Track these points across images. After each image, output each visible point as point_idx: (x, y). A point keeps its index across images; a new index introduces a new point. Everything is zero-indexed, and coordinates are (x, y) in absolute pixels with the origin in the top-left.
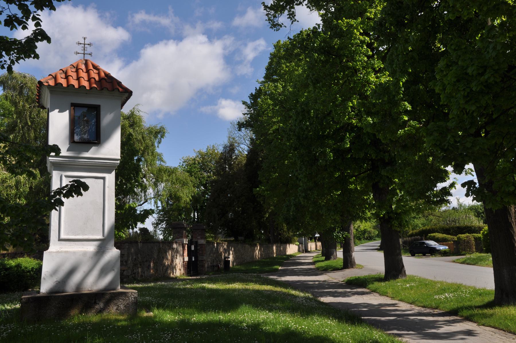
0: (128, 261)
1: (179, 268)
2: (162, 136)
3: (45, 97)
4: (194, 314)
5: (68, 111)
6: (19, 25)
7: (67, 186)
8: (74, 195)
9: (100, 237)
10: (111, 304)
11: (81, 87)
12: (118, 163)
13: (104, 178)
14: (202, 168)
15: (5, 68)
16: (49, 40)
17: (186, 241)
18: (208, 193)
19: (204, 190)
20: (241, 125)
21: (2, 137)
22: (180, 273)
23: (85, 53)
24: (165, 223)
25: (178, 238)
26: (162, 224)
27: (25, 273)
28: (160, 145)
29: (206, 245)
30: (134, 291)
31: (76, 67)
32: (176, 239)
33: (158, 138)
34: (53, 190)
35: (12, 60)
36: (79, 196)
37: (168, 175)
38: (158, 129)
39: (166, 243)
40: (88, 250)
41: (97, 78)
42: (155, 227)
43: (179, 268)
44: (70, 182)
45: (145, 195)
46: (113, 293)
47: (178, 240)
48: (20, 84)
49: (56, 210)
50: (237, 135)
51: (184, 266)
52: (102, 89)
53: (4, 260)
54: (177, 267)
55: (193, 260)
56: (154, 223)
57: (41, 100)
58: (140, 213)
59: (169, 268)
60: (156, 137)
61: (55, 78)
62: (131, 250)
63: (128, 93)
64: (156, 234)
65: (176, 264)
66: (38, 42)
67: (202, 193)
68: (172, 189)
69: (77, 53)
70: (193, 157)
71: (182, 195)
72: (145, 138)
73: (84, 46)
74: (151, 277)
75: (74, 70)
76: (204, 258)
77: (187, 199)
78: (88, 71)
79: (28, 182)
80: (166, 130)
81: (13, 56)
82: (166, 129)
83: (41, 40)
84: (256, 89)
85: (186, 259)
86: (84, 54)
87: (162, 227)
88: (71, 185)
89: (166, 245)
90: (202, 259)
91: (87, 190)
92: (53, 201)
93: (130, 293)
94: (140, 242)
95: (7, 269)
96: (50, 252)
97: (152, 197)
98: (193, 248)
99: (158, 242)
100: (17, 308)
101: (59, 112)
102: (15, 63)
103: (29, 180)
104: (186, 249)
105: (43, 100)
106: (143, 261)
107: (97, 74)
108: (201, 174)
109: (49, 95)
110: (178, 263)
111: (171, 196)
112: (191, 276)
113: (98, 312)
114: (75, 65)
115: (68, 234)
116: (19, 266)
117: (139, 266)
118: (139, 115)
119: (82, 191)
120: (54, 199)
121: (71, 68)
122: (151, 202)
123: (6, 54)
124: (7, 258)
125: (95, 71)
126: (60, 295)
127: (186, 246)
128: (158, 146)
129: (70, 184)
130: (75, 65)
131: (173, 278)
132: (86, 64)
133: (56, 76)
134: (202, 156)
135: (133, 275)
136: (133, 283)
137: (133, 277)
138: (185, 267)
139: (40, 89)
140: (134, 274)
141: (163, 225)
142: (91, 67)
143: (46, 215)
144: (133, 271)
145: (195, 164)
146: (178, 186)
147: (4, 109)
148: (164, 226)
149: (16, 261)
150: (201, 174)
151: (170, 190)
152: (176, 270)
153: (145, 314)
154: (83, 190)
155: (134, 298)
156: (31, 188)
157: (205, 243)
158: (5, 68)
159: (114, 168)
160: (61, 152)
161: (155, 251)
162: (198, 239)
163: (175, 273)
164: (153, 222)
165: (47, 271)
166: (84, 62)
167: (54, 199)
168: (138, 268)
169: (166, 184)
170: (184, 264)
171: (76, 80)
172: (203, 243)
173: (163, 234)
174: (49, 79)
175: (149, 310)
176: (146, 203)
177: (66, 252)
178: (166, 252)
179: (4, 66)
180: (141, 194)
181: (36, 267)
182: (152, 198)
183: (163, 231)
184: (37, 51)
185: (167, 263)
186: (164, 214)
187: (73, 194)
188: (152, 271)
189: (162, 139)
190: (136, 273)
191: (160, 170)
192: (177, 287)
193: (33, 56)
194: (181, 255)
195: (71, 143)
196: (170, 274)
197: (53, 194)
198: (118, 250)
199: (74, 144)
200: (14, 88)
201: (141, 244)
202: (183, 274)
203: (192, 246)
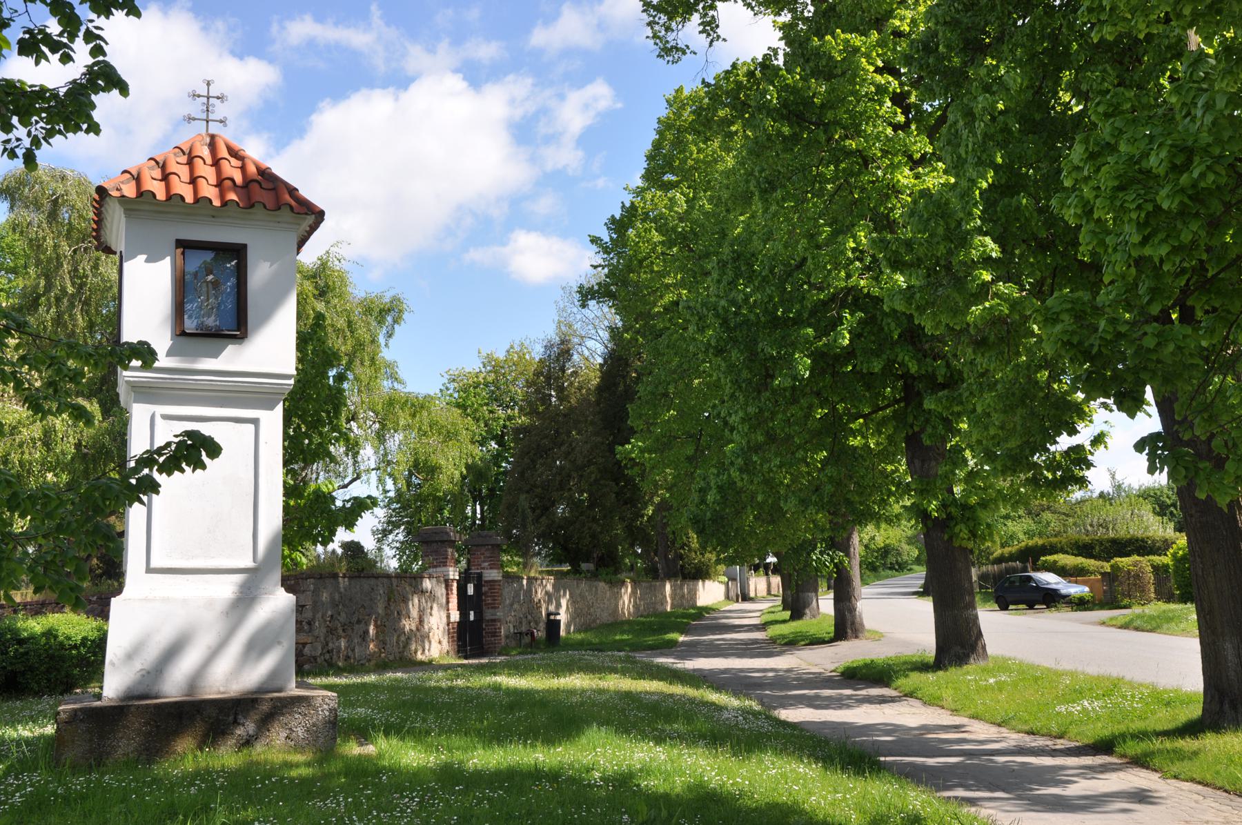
3: (112, 222)
5: (168, 259)
6: (54, 51)
7: (168, 444)
12: (290, 385)
13: (255, 422)
16: (123, 89)
17: (453, 574)
20: (586, 295)
25: (435, 567)
28: (391, 341)
31: (187, 152)
35: (36, 136)
36: (199, 471)
38: (386, 303)
41: (238, 178)
42: (379, 541)
45: (355, 462)
49: (142, 502)
50: (579, 317)
52: (252, 206)
57: (102, 232)
60: (381, 322)
61: (138, 179)
63: (313, 216)
69: (190, 119)
71: (442, 462)
74: (369, 660)
75: (184, 159)
78: (216, 163)
80: (405, 306)
81: (38, 126)
83: (106, 89)
84: (623, 206)
85: (455, 616)
88: (178, 444)
90: (493, 617)
92: (133, 481)
94: (344, 574)
95: (21, 642)
97: (373, 466)
98: (471, 590)
101: (147, 261)
104: (455, 591)
109: (123, 219)
110: (435, 627)
116: (52, 634)
121: (175, 154)
122: (368, 479)
123: (20, 122)
125: (234, 162)
127: (455, 584)
128: (386, 345)
129: (177, 440)
131: (422, 663)
132: (213, 145)
135: (327, 656)
136: (327, 675)
139: (101, 206)
140: (328, 652)
142: (223, 153)
146: (433, 440)
147: (13, 255)
148: (401, 537)
152: (430, 642)
156: (78, 446)
157: (500, 578)
162: (484, 568)
166: (208, 140)
168: (339, 638)
171: (189, 183)
172: (496, 578)
174: (122, 183)
177: (165, 600)
178: (405, 600)
181: (93, 635)
183: (397, 548)
184: (96, 115)
185: (407, 628)
187: (184, 465)
189: (396, 326)
190: (332, 650)
191: (391, 402)
192: (433, 684)
193: (85, 126)
194: (441, 606)
196: (416, 652)
197: (132, 464)
199: (182, 339)
201: (346, 579)
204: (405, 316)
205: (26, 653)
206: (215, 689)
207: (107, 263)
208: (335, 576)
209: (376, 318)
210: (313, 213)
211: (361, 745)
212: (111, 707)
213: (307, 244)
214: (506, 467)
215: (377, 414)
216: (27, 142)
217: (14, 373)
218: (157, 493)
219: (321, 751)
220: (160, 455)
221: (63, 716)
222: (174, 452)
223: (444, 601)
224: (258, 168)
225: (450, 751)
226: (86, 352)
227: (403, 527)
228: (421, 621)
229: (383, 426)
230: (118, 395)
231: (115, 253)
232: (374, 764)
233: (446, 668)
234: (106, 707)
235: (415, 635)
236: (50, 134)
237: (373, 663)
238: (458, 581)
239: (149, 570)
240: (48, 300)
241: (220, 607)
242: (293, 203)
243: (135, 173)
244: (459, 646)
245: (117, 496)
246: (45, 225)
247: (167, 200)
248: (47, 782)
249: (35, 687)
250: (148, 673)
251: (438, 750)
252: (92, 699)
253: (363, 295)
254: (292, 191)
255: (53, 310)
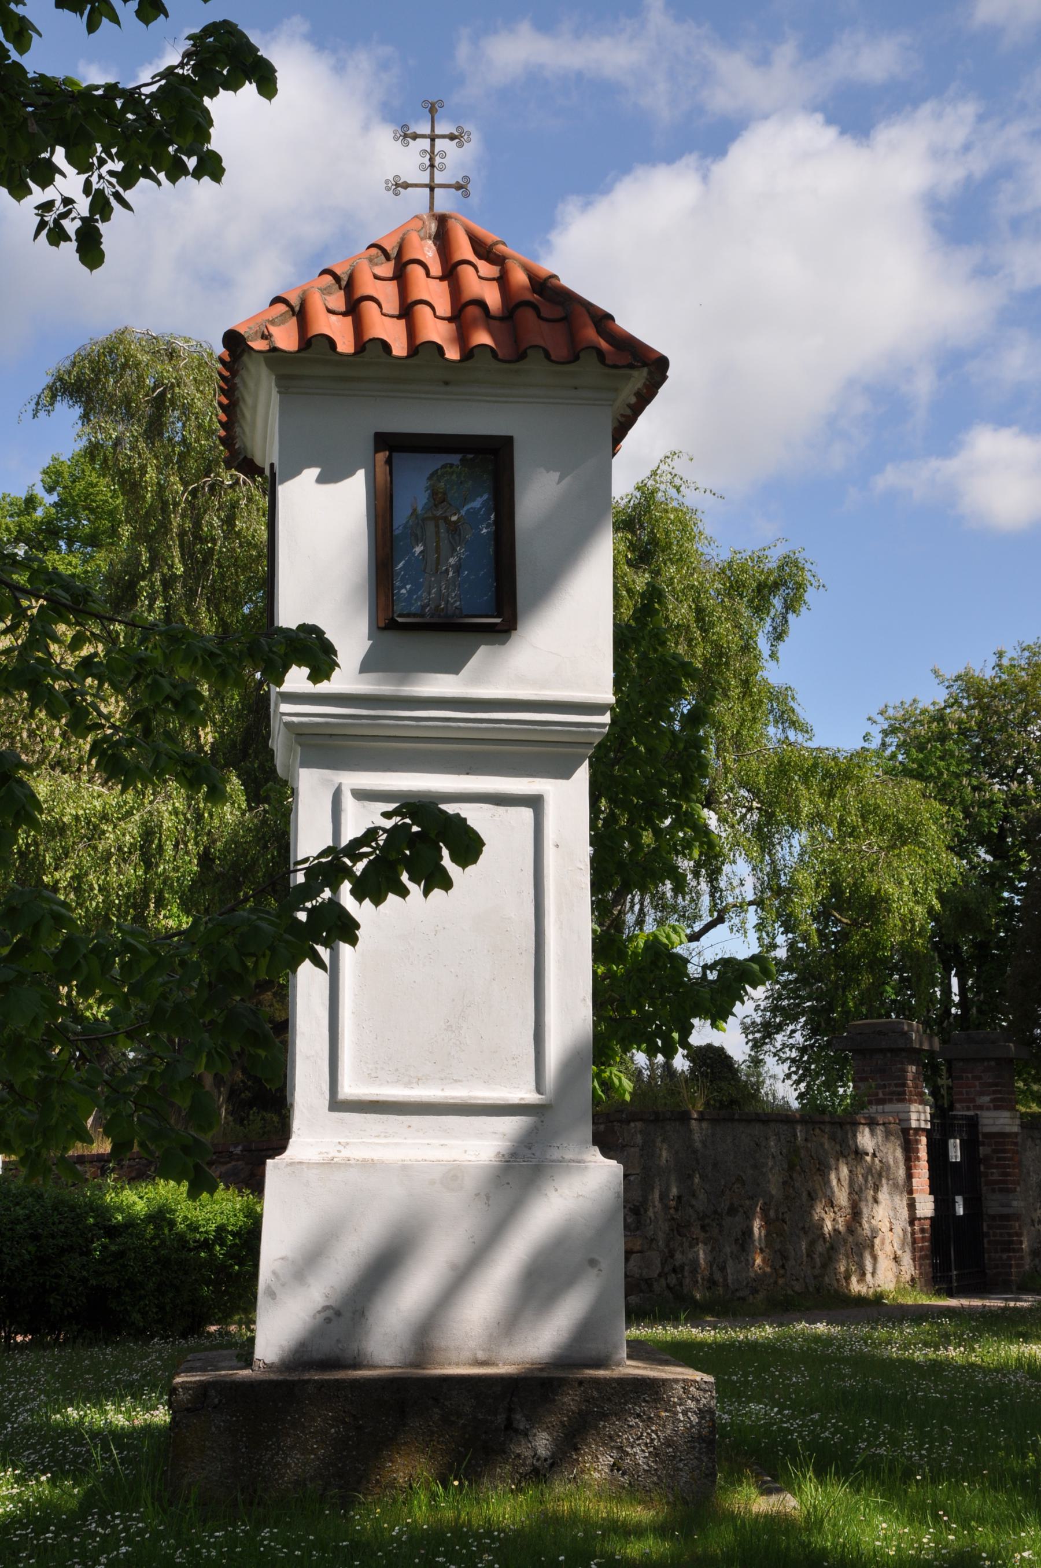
0: (646, 1211)
1: (888, 1248)
2: (790, 606)
3: (254, 408)
4: (1022, 1523)
5: (361, 474)
7: (371, 834)
8: (411, 886)
9: (527, 1094)
10: (584, 1440)
11: (417, 348)
12: (602, 725)
13: (535, 802)
14: (978, 756)
15: (68, 238)
17: (920, 1116)
18: (1011, 881)
19: (991, 865)
21: (67, 591)
22: (898, 1277)
23: (438, 180)
24: (806, 1023)
25: (882, 1102)
26: (791, 1027)
27: (190, 1250)
28: (782, 647)
29: (1019, 1140)
30: (698, 1376)
31: (393, 254)
32: (870, 1103)
33: (772, 613)
34: (299, 858)
35: (100, 192)
36: (437, 893)
37: (821, 794)
38: (770, 572)
39: (823, 1123)
40: (467, 1157)
41: (492, 297)
42: (757, 1045)
43: (888, 1248)
44: (387, 815)
45: (714, 890)
46: (596, 1382)
47: (880, 1108)
48: (154, 390)
49: (318, 962)
51: (914, 1241)
52: (521, 356)
53: (100, 1187)
54: (883, 1243)
55: (960, 1211)
56: (753, 1023)
57: (238, 430)
58: (704, 974)
59: (842, 1251)
60: (760, 609)
61: (301, 314)
62: (660, 1155)
63: (645, 371)
64: (759, 1075)
65: (875, 1232)
66: (216, 93)
67: (984, 879)
68: (843, 858)
69: (400, 185)
70: (934, 704)
71: (890, 888)
72: (711, 614)
73: (433, 146)
74: (755, 1291)
75: (386, 269)
76: (1015, 1203)
77: (919, 909)
78: (450, 272)
79: (196, 831)
80: (808, 576)
81: (104, 170)
82: (808, 566)
83: (233, 85)
85: (926, 1207)
86: (432, 190)
87: (791, 1041)
88: (391, 832)
89: (822, 1131)
90: (1005, 1211)
91: (474, 861)
92: (302, 916)
93: (678, 1387)
94: (701, 1113)
95: (113, 1231)
96: (291, 1164)
97: (750, 896)
98: (955, 1152)
99: (782, 1117)
100: (157, 1427)
101: (321, 480)
102: (111, 209)
103: (198, 823)
104: (923, 1154)
105: (247, 429)
106: (715, 1212)
107: (495, 284)
108: (975, 789)
109: (275, 397)
110: (885, 1226)
111: (836, 889)
112: (951, 1295)
113: (524, 1476)
114: (391, 247)
115: (373, 1078)
116: (164, 1219)
117: (696, 1231)
118: (675, 504)
119: (447, 861)
120: (309, 905)
121: (371, 260)
122: (743, 922)
123: (70, 158)
124: (115, 1180)
125: (486, 269)
126: (343, 1381)
127: (924, 1140)
128: (773, 656)
129: (389, 824)
130: (391, 247)
131: (860, 1301)
132: (442, 239)
133: (303, 303)
134: (979, 697)
135: (673, 1280)
136: (676, 1321)
137: (668, 1286)
138: (922, 1249)
139: (234, 373)
140: (674, 1270)
141: (793, 1031)
142: (464, 250)
143: (264, 986)
144: (672, 1256)
145: (943, 737)
146: (872, 844)
147: (92, 511)
148: (799, 1038)
149: (150, 1195)
150: (975, 789)
151: (831, 863)
152: (875, 1258)
153: (762, 1504)
154: (454, 859)
155: (701, 1413)
156: (205, 859)
157: (1015, 1129)
158: (68, 238)
159: (581, 750)
160: (339, 660)
161: (770, 1164)
162: (981, 1108)
163: (873, 1274)
164: (748, 1021)
165: (282, 1259)
166: (433, 227)
167: (309, 905)
168: (694, 1243)
169: (813, 838)
170: (913, 1233)
171: (399, 317)
172: (1008, 1129)
173: (794, 1077)
174: (272, 322)
175: (775, 1478)
176: (722, 929)
177: (367, 1165)
178: (823, 1170)
179: (61, 228)
180: (694, 883)
181: (237, 1222)
182: (751, 903)
183: (793, 1061)
184: (218, 142)
185: (828, 1226)
186: (796, 981)
187: (405, 877)
188: (758, 1261)
189: (791, 617)
190: (682, 1267)
191: (783, 769)
192: (894, 1352)
193: (192, 163)
194: (896, 1186)
195: (379, 628)
196: (848, 1278)
197: (300, 878)
198: (614, 1162)
199: (390, 636)
200: (126, 408)
201: (704, 1125)
202: (913, 1279)
203: (951, 1141)
204: (810, 595)
205: (121, 1254)
206: (466, 1355)
207: (250, 512)
208: (684, 1117)
209: (751, 601)
210: (645, 364)
211: (767, 1492)
212: (271, 1382)
213: (641, 419)
214: (1011, 900)
215: (756, 793)
216: (83, 206)
217: (69, 694)
218: (353, 940)
219: (686, 1503)
220: (356, 858)
221: (182, 1396)
222: (382, 849)
223: (901, 1172)
224: (532, 276)
225: (965, 1524)
226: (205, 650)
227: (803, 1020)
228: (856, 1214)
229: (769, 817)
230: (275, 766)
231: (260, 471)
232: (802, 1544)
233: (918, 1315)
234: (261, 1383)
235: (845, 1241)
236: (127, 179)
237: (761, 1296)
238: (928, 1133)
239: (337, 1104)
240: (152, 585)
241: (470, 1184)
242: (604, 345)
243: (295, 301)
244: (934, 1266)
245: (272, 948)
246: (142, 445)
247: (356, 353)
248: (157, 1536)
249: (136, 1317)
250: (338, 1313)
251: (936, 1518)
252: (234, 1363)
253: (725, 555)
254: (603, 320)
255: (159, 603)
